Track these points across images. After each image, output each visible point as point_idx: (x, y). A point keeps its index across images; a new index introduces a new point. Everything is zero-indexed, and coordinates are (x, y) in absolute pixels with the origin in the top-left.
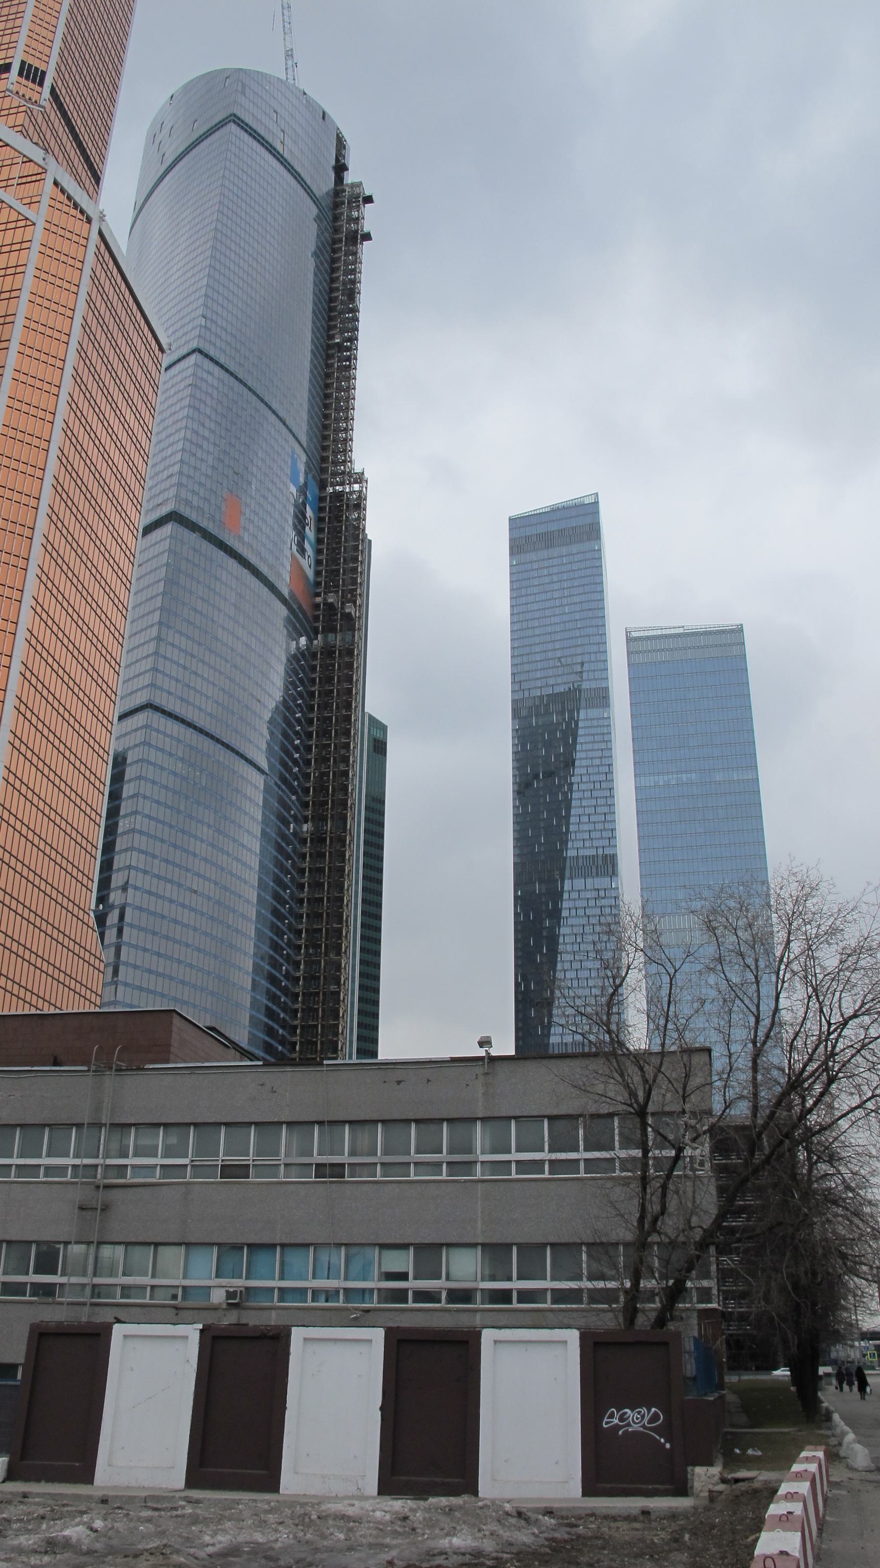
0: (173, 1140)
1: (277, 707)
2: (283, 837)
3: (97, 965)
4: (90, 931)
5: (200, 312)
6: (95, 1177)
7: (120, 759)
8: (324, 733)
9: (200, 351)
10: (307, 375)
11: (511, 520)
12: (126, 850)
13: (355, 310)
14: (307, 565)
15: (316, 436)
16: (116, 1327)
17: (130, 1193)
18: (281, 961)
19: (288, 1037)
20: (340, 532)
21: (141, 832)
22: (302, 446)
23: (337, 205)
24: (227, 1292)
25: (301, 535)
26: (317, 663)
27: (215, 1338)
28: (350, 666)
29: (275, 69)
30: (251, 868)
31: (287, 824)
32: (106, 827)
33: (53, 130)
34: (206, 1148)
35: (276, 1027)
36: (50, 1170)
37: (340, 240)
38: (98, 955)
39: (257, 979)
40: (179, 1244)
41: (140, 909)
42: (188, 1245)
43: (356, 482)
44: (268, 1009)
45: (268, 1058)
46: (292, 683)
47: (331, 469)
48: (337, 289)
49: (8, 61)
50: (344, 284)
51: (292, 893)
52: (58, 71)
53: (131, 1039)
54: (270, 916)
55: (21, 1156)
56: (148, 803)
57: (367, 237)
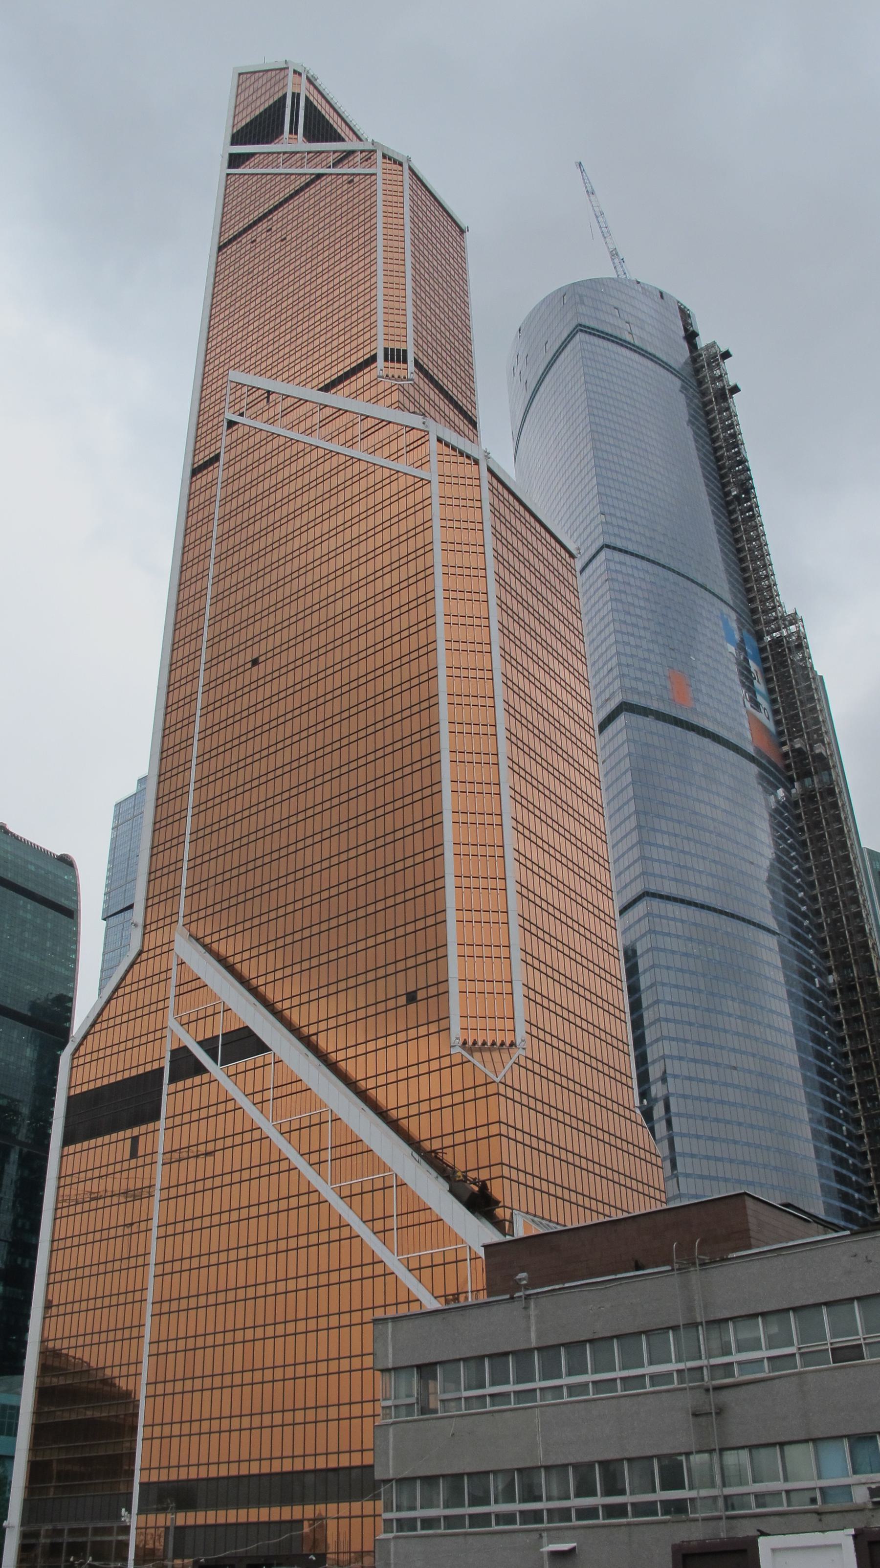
0: (774, 1329)
1: (772, 865)
2: (811, 993)
3: (654, 1162)
4: (640, 1128)
5: (598, 510)
6: (703, 1380)
7: (630, 953)
8: (826, 879)
9: (608, 546)
10: (715, 537)
12: (657, 1041)
13: (743, 461)
14: (765, 717)
15: (740, 591)
16: (762, 1540)
17: (743, 1391)
18: (840, 1121)
19: (866, 1200)
20: (789, 676)
21: (667, 1020)
22: (728, 605)
23: (697, 371)
24: (869, 1489)
25: (751, 689)
26: (801, 811)
27: (872, 1544)
28: (835, 805)
29: (606, 271)
30: (785, 1033)
31: (811, 979)
32: (633, 1022)
33: (424, 395)
34: (811, 1333)
35: (850, 1191)
36: (655, 1378)
37: (711, 402)
38: (653, 1151)
39: (819, 1145)
40: (806, 1441)
41: (684, 1096)
42: (814, 1440)
43: (791, 624)
44: (837, 1174)
45: (850, 1226)
46: (781, 837)
47: (763, 618)
48: (721, 447)
49: (373, 353)
50: (726, 440)
51: (834, 1049)
52: (417, 344)
53: (709, 1230)
54: (817, 1078)
55: (624, 1368)
56: (667, 989)
57: (735, 389)
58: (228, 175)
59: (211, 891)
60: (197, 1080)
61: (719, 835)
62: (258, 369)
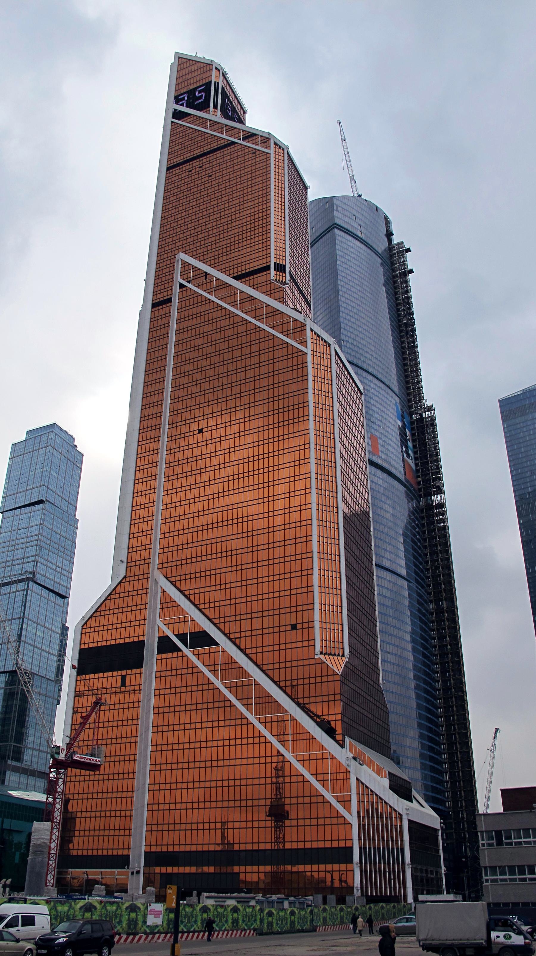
8: (434, 553)
11: (500, 401)
14: (411, 462)
23: (391, 256)
48: (400, 304)
49: (268, 264)
57: (411, 271)
58: (172, 122)
59: (175, 553)
60: (175, 654)
61: (389, 528)
62: (194, 253)
